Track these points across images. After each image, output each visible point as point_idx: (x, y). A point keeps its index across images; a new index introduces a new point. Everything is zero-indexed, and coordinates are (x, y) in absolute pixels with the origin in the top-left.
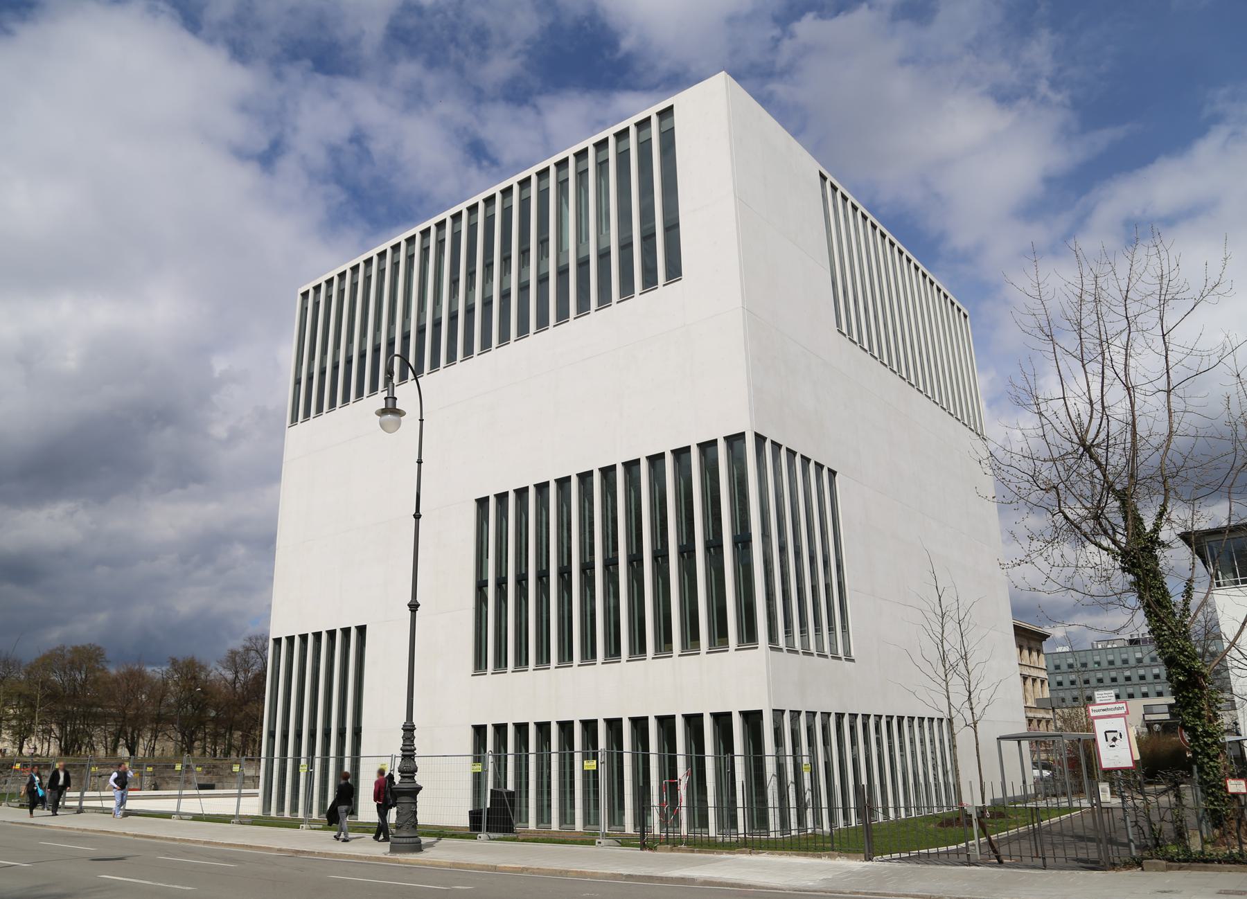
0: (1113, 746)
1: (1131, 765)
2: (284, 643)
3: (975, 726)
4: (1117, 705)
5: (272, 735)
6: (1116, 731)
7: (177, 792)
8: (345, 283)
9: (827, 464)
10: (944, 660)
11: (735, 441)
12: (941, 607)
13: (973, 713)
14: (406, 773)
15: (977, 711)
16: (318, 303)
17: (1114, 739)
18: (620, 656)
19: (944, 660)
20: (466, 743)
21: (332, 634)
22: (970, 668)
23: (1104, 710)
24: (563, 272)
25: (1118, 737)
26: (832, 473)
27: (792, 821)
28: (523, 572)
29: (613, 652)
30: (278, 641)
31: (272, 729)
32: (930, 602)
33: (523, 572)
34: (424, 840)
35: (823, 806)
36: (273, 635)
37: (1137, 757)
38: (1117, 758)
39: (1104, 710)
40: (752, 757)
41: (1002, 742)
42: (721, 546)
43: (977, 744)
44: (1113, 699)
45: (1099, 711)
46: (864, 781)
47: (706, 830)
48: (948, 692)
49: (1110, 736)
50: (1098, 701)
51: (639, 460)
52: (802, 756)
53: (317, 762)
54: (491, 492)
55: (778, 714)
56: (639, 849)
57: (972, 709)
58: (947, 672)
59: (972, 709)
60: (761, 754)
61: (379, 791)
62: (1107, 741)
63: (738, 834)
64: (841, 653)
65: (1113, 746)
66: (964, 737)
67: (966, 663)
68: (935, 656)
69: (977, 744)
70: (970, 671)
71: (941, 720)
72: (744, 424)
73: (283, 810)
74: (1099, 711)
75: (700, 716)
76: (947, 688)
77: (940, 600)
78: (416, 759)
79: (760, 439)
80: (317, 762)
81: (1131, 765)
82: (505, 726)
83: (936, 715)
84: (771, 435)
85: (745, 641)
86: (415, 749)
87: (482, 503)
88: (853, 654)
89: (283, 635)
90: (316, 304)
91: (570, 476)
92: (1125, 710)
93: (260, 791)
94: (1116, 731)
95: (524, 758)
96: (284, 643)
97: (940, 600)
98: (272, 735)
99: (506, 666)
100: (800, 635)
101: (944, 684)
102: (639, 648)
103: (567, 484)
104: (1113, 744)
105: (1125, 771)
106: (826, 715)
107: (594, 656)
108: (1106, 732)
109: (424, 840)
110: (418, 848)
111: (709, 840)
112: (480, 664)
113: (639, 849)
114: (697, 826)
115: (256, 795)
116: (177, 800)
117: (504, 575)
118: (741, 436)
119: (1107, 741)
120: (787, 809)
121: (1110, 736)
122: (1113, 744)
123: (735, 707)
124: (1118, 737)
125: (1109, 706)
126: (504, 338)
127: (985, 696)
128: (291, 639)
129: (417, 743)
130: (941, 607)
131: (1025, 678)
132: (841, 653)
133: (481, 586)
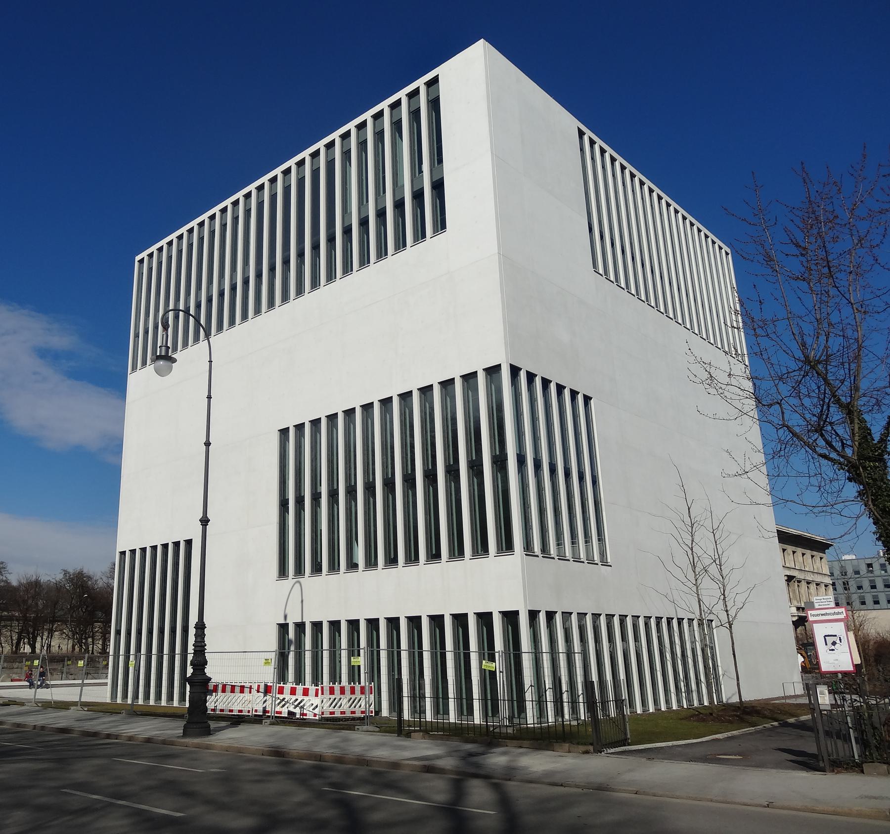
0: (833, 650)
1: (851, 668)
2: (128, 554)
3: (731, 627)
4: (837, 610)
5: (118, 632)
6: (836, 636)
7: (80, 682)
8: (204, 228)
9: (582, 390)
10: (694, 566)
11: (493, 371)
12: (690, 517)
13: (728, 615)
14: (197, 666)
15: (732, 613)
16: (192, 244)
17: (834, 643)
18: (441, 558)
19: (694, 566)
20: (272, 643)
21: (165, 546)
22: (724, 573)
23: (822, 615)
24: (399, 205)
25: (838, 641)
26: (587, 399)
27: (549, 714)
28: (371, 480)
29: (334, 567)
30: (123, 553)
31: (118, 629)
32: (679, 513)
33: (371, 480)
34: (213, 725)
35: (548, 699)
36: (120, 549)
37: (858, 661)
38: (836, 662)
39: (822, 615)
40: (512, 655)
41: (826, 638)
42: (481, 465)
43: (733, 644)
44: (833, 605)
45: (818, 615)
46: (595, 678)
47: (472, 717)
48: (698, 595)
49: (830, 640)
50: (817, 606)
51: (432, 385)
52: (559, 653)
53: (143, 658)
54: (291, 424)
55: (533, 615)
56: (397, 735)
57: (727, 611)
58: (697, 576)
59: (727, 611)
60: (519, 651)
61: (864, 650)
62: (826, 644)
63: (527, 724)
64: (597, 558)
65: (833, 650)
66: (720, 637)
67: (721, 569)
68: (684, 562)
69: (733, 644)
70: (724, 576)
71: (691, 620)
72: (500, 357)
73: (149, 698)
74: (818, 615)
75: (490, 614)
76: (697, 591)
77: (689, 512)
78: (206, 654)
79: (515, 371)
80: (143, 658)
81: (851, 668)
82: (339, 622)
83: (685, 615)
84: (526, 366)
85: (504, 549)
86: (206, 646)
87: (284, 432)
88: (609, 560)
89: (127, 550)
90: (190, 246)
91: (355, 408)
92: (845, 615)
93: (109, 681)
94: (836, 636)
95: (395, 653)
96: (128, 554)
97: (689, 512)
98: (118, 632)
99: (339, 569)
100: (597, 538)
101: (694, 589)
102: (457, 551)
103: (408, 399)
104: (833, 647)
105: (845, 674)
106: (582, 616)
107: (417, 558)
108: (826, 636)
109: (213, 725)
110: (208, 732)
111: (474, 727)
112: (283, 572)
113: (397, 735)
114: (465, 713)
115: (106, 684)
116: (80, 687)
117: (335, 488)
118: (498, 368)
119: (826, 644)
120: (545, 703)
121: (830, 640)
122: (833, 647)
123: (496, 608)
124: (838, 641)
125: (828, 611)
126: (347, 269)
127: (740, 599)
128: (133, 552)
129: (207, 640)
130: (690, 517)
131: (790, 579)
132: (597, 558)
133: (284, 504)
